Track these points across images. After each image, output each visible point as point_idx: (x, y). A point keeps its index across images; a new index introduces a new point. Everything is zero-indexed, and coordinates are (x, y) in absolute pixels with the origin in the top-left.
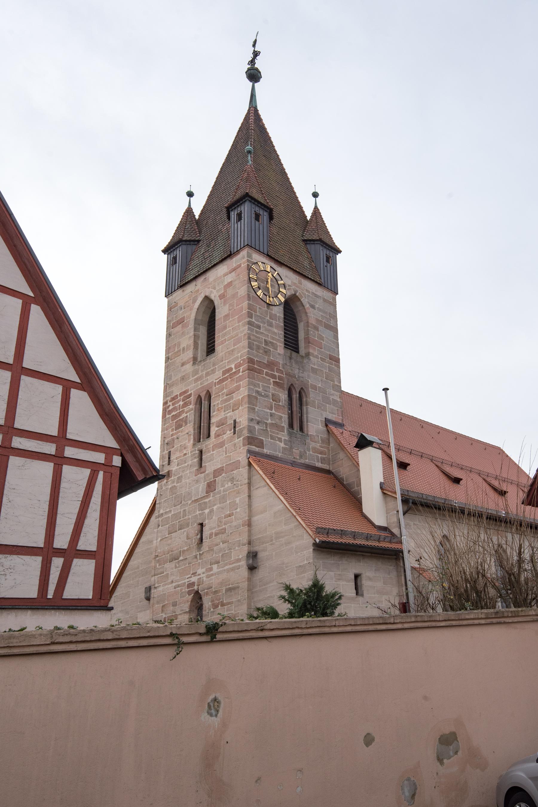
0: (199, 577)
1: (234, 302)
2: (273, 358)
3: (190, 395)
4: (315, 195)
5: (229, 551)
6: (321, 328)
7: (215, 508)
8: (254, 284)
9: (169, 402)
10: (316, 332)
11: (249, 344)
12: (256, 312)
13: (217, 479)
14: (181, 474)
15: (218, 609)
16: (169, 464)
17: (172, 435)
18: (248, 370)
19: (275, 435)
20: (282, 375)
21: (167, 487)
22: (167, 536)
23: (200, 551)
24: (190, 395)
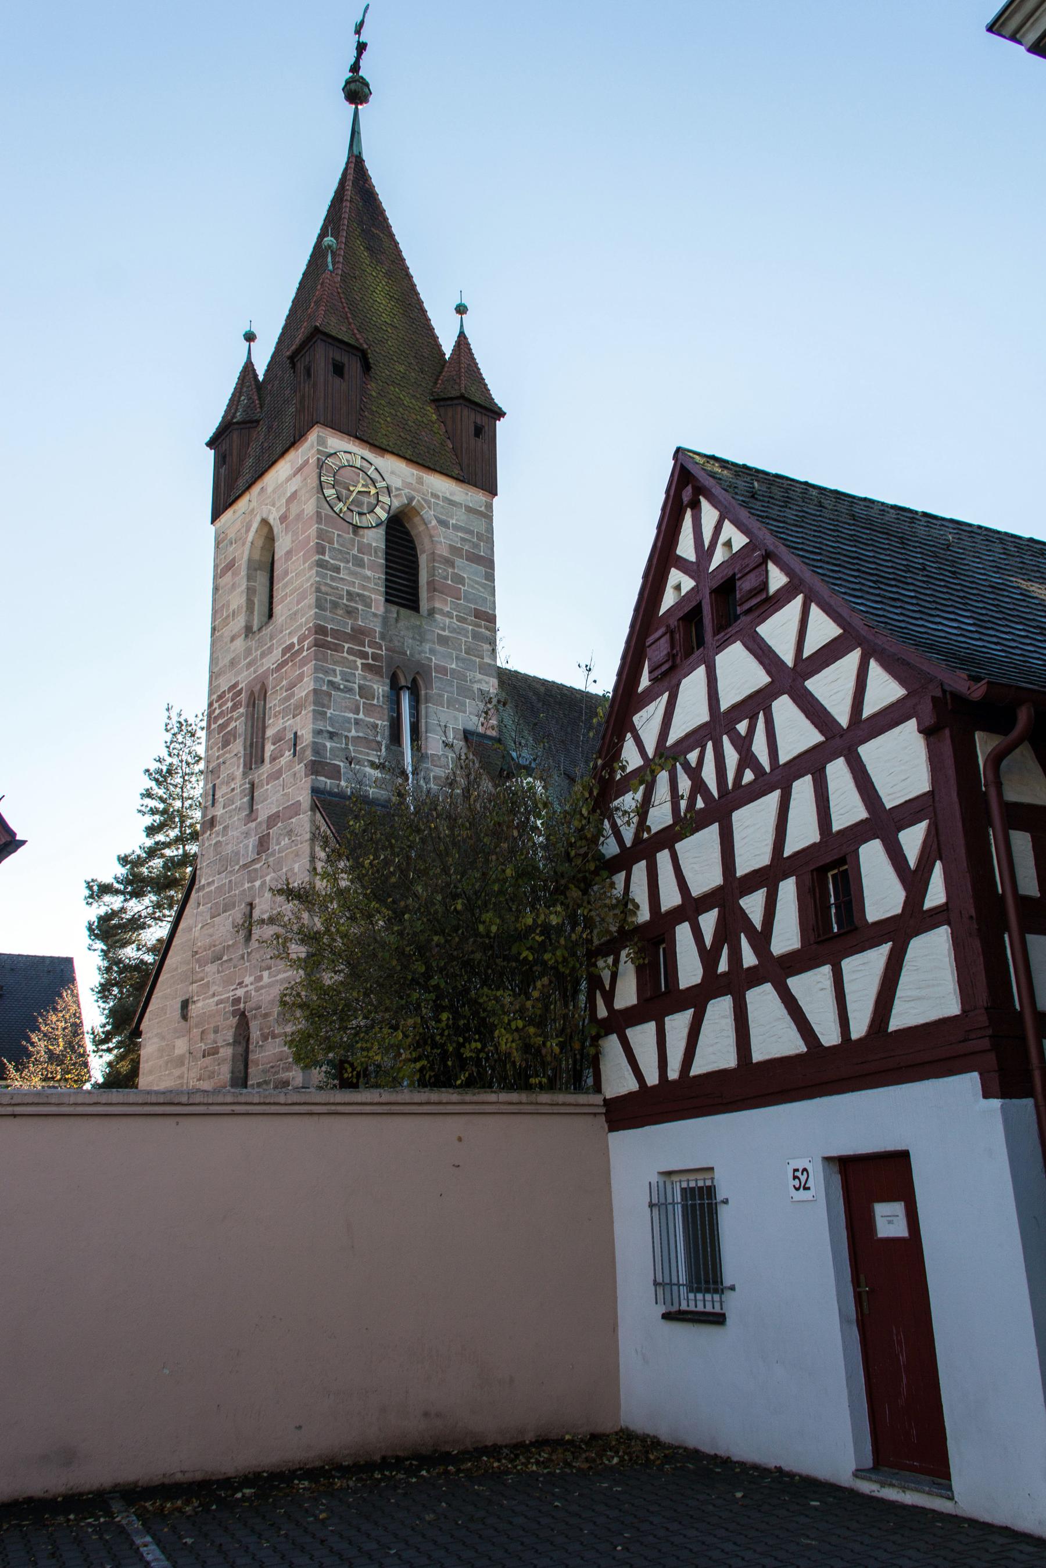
0: (246, 989)
1: (298, 528)
3: (240, 692)
4: (461, 310)
6: (459, 562)
12: (331, 542)
16: (213, 805)
17: (218, 758)
18: (316, 645)
20: (380, 652)
24: (240, 692)
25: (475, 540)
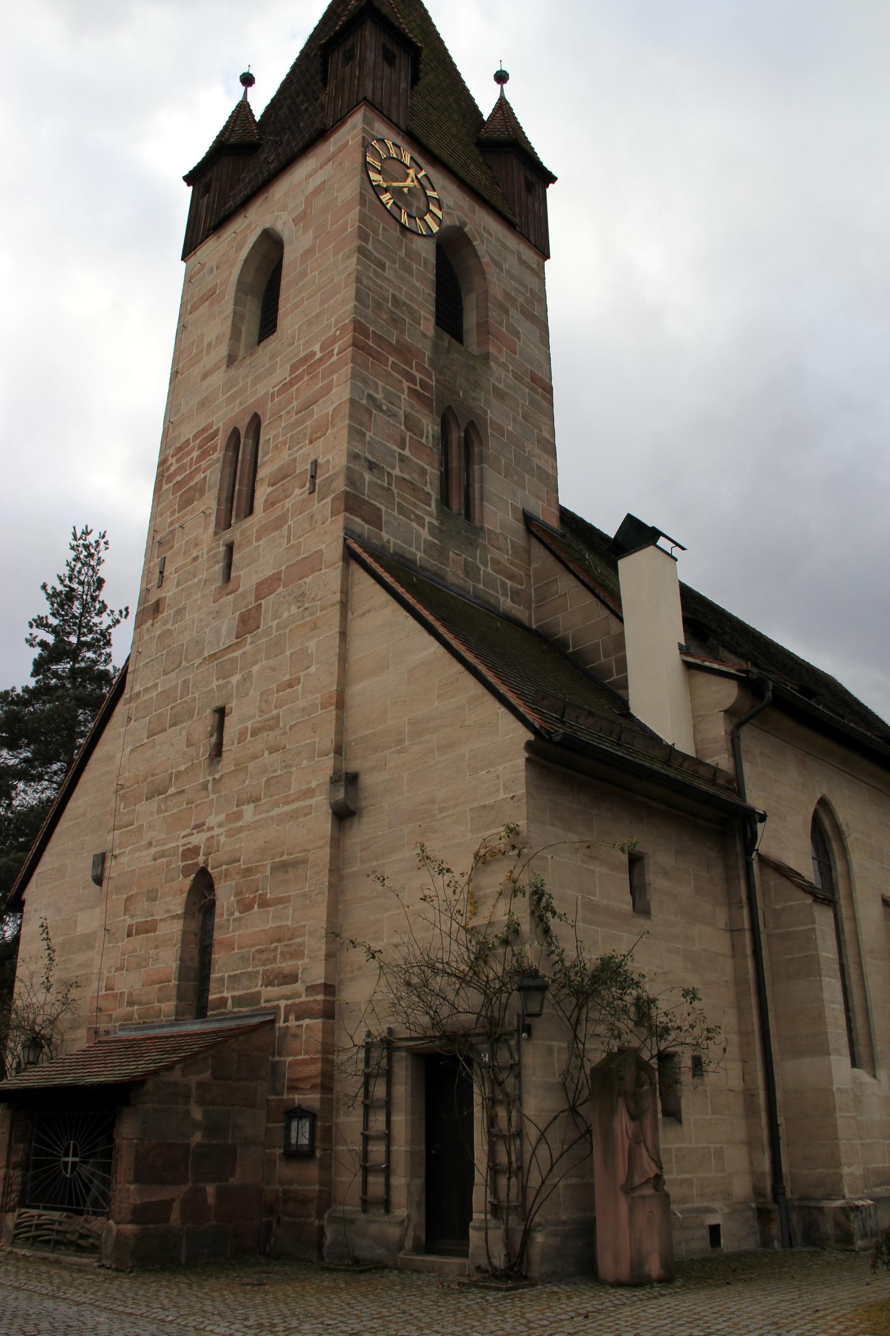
2: (409, 338)
4: (501, 77)
5: (286, 771)
6: (512, 312)
7: (255, 669)
9: (170, 457)
11: (356, 292)
13: (263, 602)
14: (183, 603)
15: (251, 914)
17: (171, 524)
19: (410, 507)
21: (153, 634)
22: (145, 741)
23: (216, 772)
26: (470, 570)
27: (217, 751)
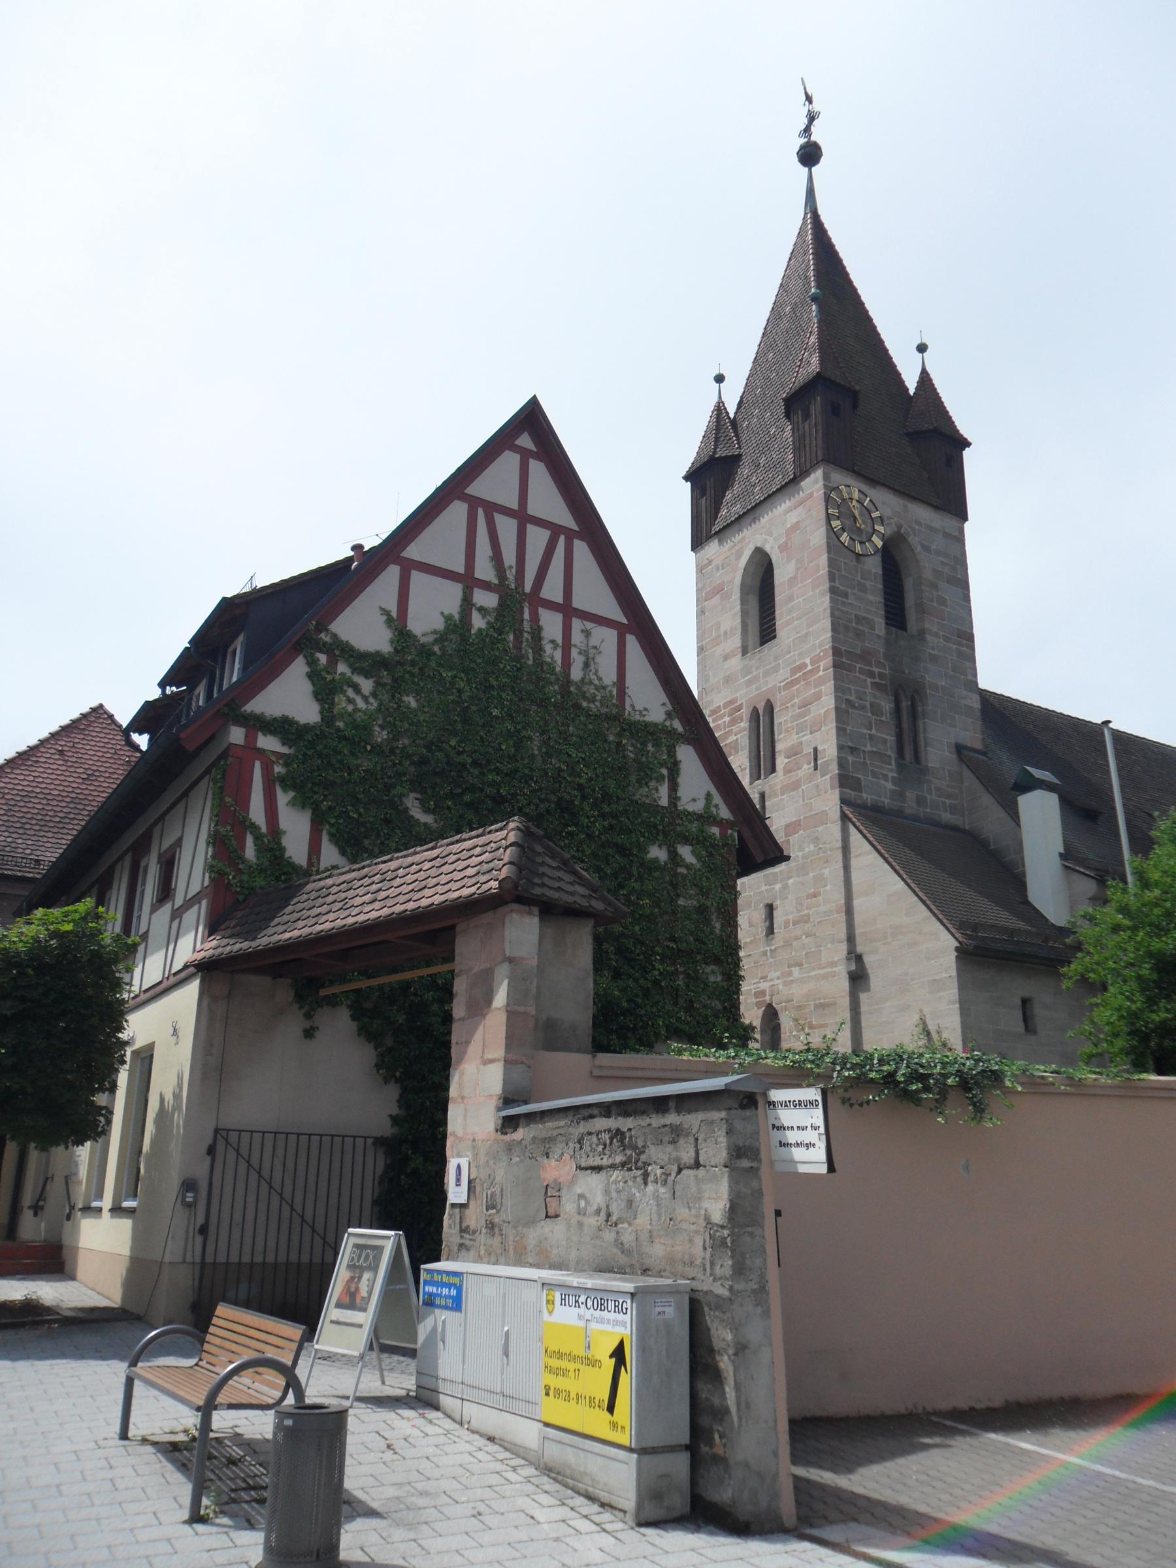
0: (771, 983)
3: (739, 708)
4: (922, 348)
7: (790, 882)
8: (836, 524)
10: (935, 593)
24: (739, 708)
25: (953, 563)
26: (920, 801)
27: (770, 931)
